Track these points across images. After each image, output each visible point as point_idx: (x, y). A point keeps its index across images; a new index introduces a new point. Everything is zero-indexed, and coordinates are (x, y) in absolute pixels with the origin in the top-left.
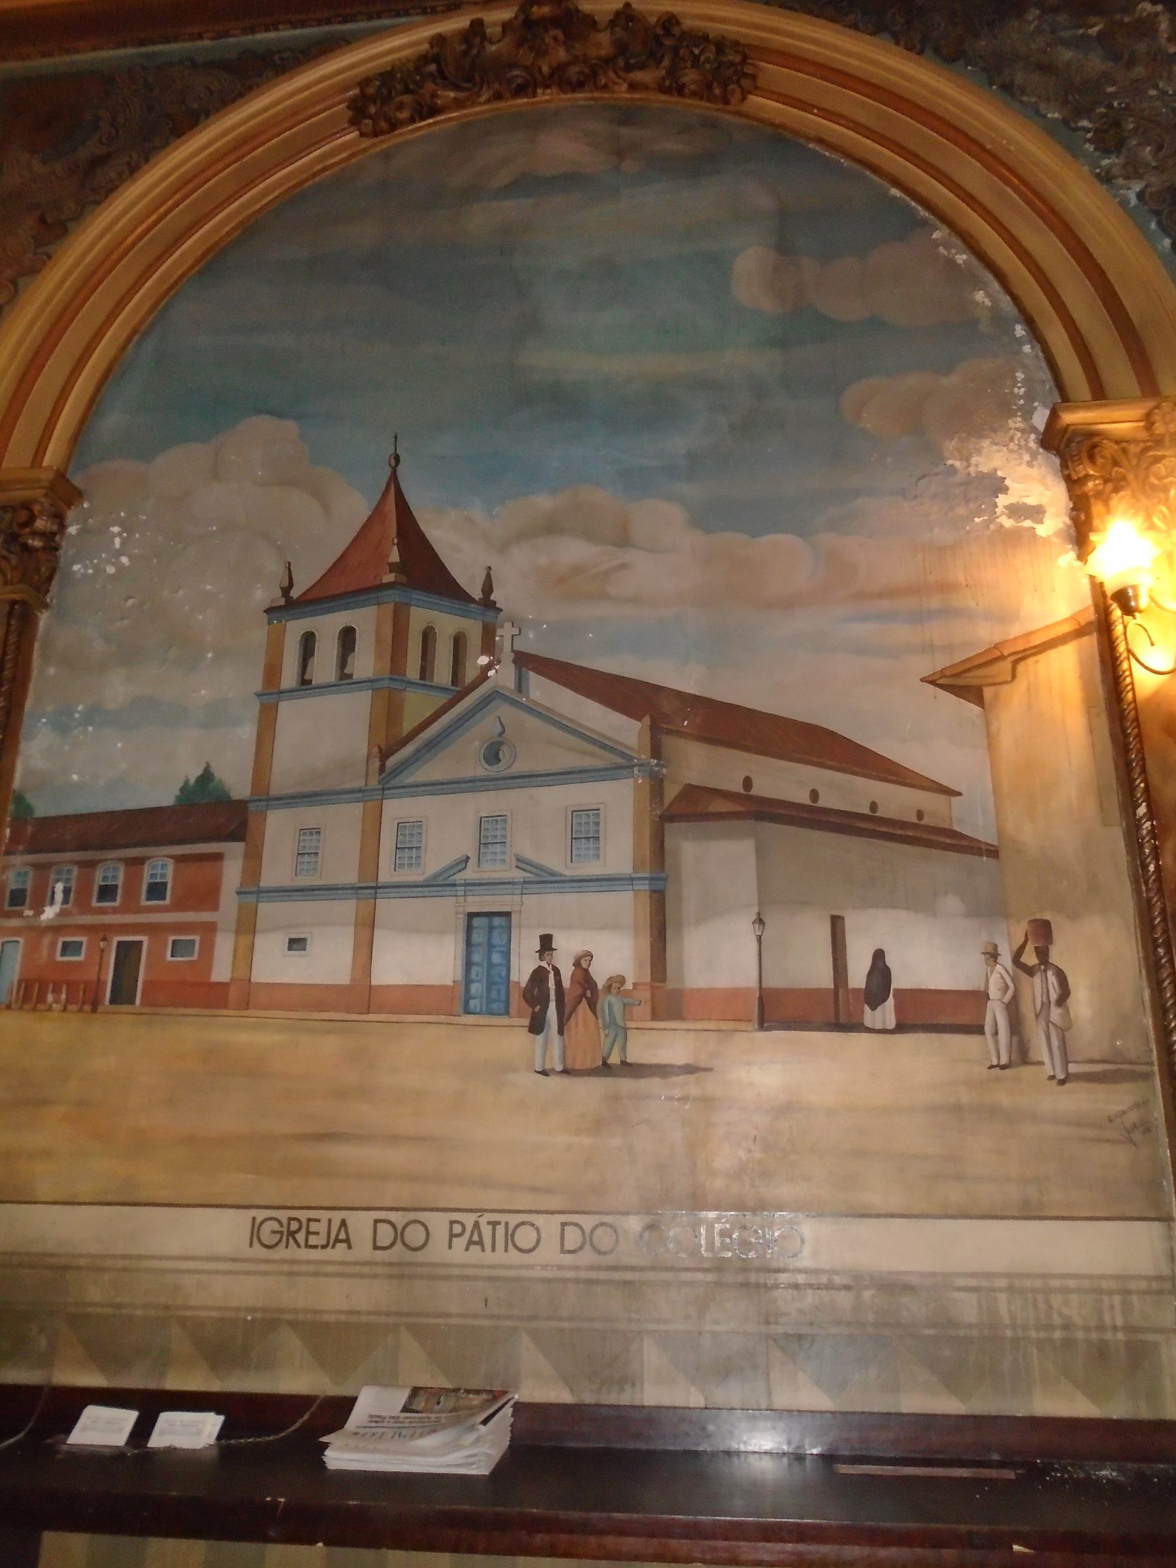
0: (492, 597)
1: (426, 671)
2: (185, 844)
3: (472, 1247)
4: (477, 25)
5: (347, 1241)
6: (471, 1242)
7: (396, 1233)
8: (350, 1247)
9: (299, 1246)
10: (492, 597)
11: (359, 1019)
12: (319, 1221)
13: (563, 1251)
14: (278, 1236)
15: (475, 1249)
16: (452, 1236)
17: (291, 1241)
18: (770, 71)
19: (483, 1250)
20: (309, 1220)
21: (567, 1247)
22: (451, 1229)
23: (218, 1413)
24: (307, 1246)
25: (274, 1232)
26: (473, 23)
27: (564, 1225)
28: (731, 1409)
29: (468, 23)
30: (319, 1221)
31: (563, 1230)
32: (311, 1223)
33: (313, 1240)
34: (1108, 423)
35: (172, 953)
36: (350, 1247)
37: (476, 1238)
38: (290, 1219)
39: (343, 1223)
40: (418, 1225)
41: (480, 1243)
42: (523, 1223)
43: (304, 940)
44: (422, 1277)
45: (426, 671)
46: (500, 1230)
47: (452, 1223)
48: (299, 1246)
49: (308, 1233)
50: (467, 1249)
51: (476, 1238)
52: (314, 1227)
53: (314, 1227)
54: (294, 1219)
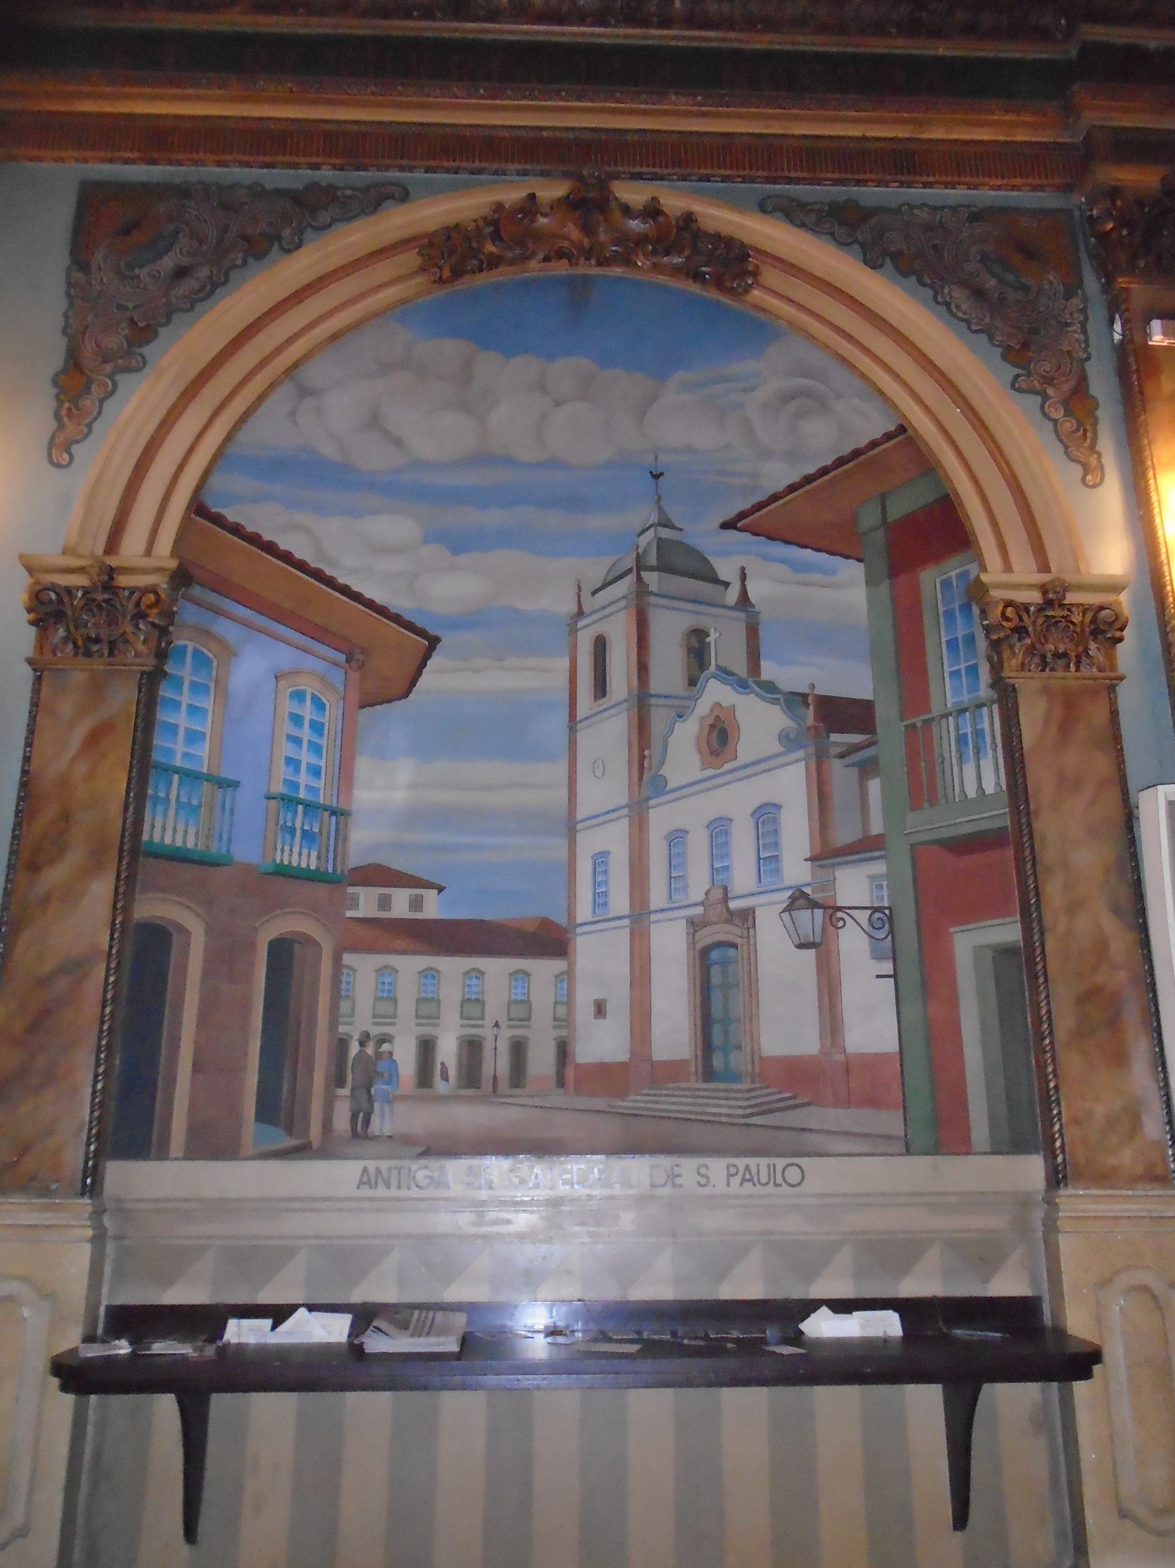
0: (160, 329)
1: (600, 899)
2: (133, 471)
3: (745, 1184)
4: (532, 196)
6: (743, 1180)
10: (160, 329)
15: (748, 1185)
16: (730, 1176)
19: (754, 1185)
22: (728, 1171)
23: (349, 1313)
28: (905, 1107)
34: (261, 398)
37: (365, 1179)
40: (800, 1178)
41: (751, 1180)
43: (64, 553)
45: (600, 899)
46: (404, 1173)
50: (358, 1188)
51: (365, 1179)
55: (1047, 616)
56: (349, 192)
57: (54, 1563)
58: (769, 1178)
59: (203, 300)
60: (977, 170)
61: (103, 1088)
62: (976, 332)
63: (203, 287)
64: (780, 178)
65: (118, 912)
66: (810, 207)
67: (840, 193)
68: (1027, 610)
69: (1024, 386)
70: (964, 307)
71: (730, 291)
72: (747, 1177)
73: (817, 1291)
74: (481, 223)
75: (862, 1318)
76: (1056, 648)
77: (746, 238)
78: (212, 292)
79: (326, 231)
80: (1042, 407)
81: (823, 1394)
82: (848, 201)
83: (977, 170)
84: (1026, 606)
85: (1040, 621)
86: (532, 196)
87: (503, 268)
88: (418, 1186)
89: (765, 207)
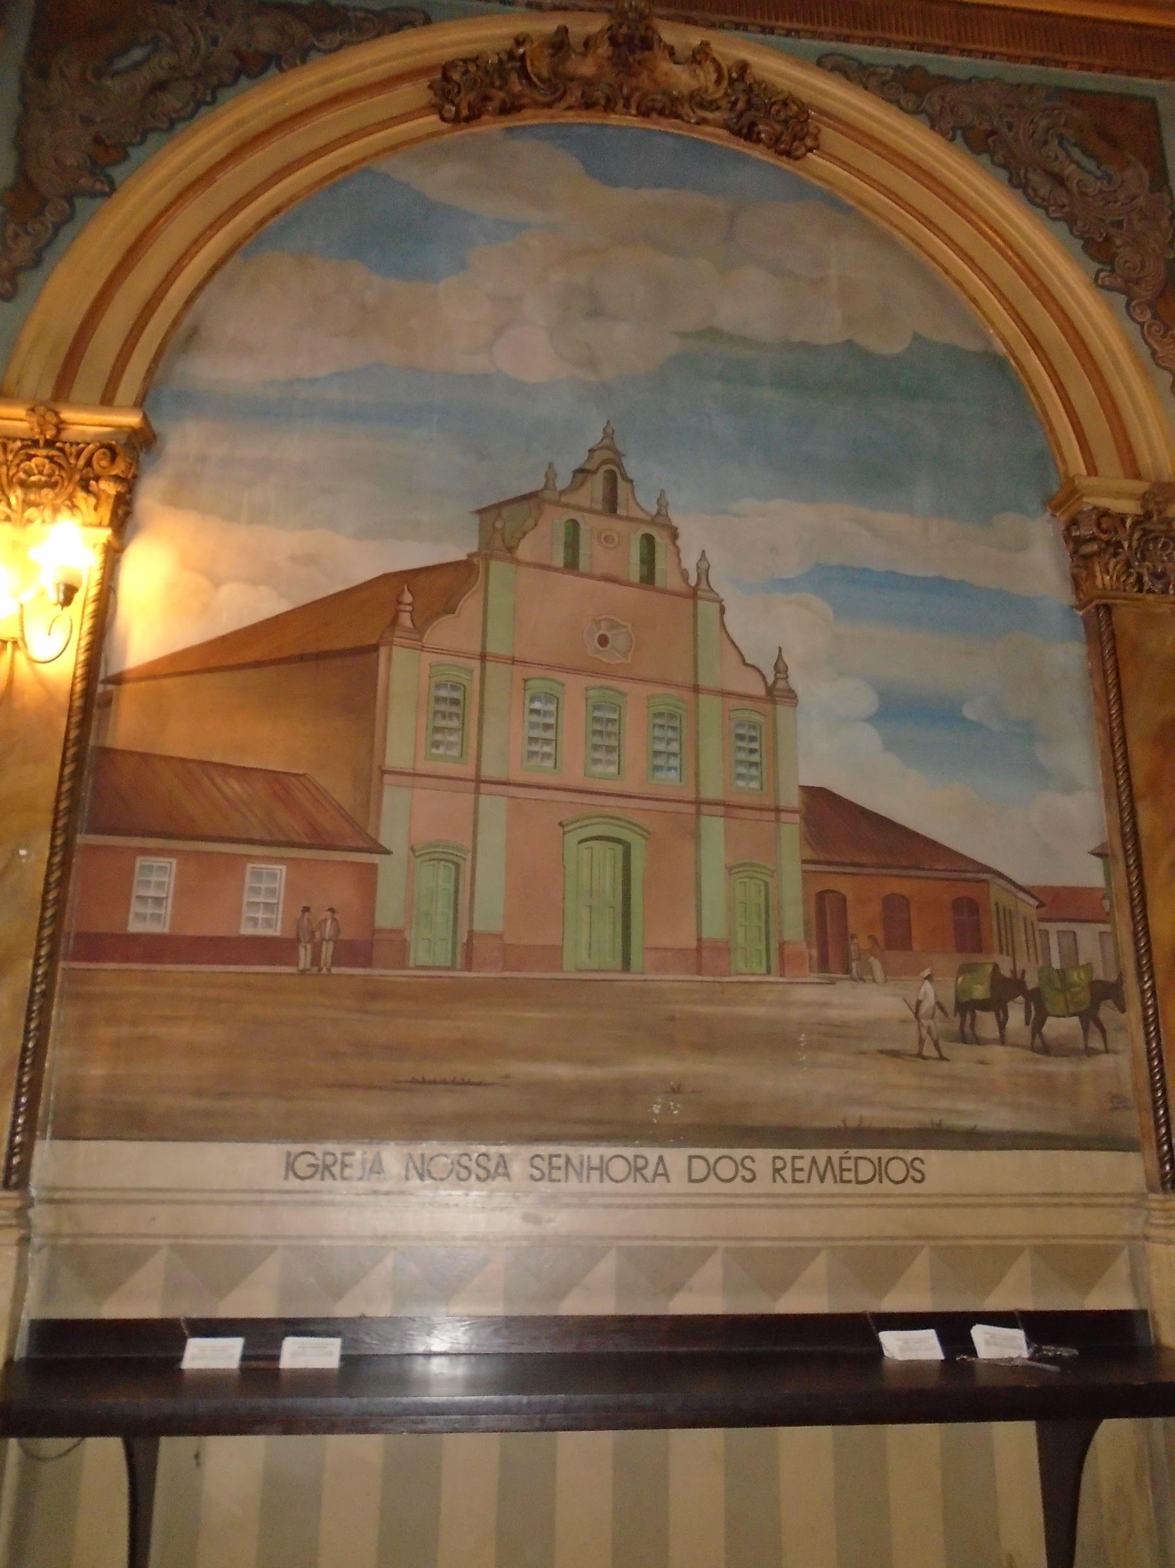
4: (564, 31)
5: (666, 1174)
7: (906, 1165)
8: (668, 1180)
9: (785, 1181)
11: (623, 978)
12: (802, 1157)
13: (691, 1180)
14: (313, 1169)
17: (638, 1175)
18: (829, 136)
20: (794, 1158)
21: (695, 1176)
24: (794, 1181)
25: (310, 1165)
26: (702, 43)
27: (691, 1158)
29: (555, 28)
30: (802, 1157)
31: (690, 1162)
32: (796, 1160)
33: (800, 1176)
35: (1064, 932)
36: (668, 1180)
38: (636, 1157)
39: (661, 1159)
42: (724, 1157)
44: (88, 1201)
47: (775, 1158)
48: (785, 1181)
49: (794, 1170)
52: (799, 1164)
53: (799, 1164)
54: (779, 1158)
55: (1144, 530)
56: (360, 14)
57: (1045, 1565)
58: (886, 1169)
59: (185, 119)
60: (911, 29)
61: (34, 1047)
62: (1055, 219)
63: (186, 105)
64: (928, 45)
65: (59, 832)
66: (871, 69)
67: (907, 57)
68: (1123, 521)
69: (1107, 282)
70: (1042, 192)
71: (788, 154)
72: (661, 1170)
73: (891, 1304)
74: (504, 57)
75: (899, 1340)
76: (1154, 566)
77: (804, 95)
78: (195, 111)
79: (333, 55)
80: (1128, 306)
81: (895, 1433)
82: (914, 68)
83: (911, 29)
84: (1122, 518)
85: (1136, 535)
86: (564, 31)
87: (527, 113)
88: (296, 1175)
89: (823, 63)
